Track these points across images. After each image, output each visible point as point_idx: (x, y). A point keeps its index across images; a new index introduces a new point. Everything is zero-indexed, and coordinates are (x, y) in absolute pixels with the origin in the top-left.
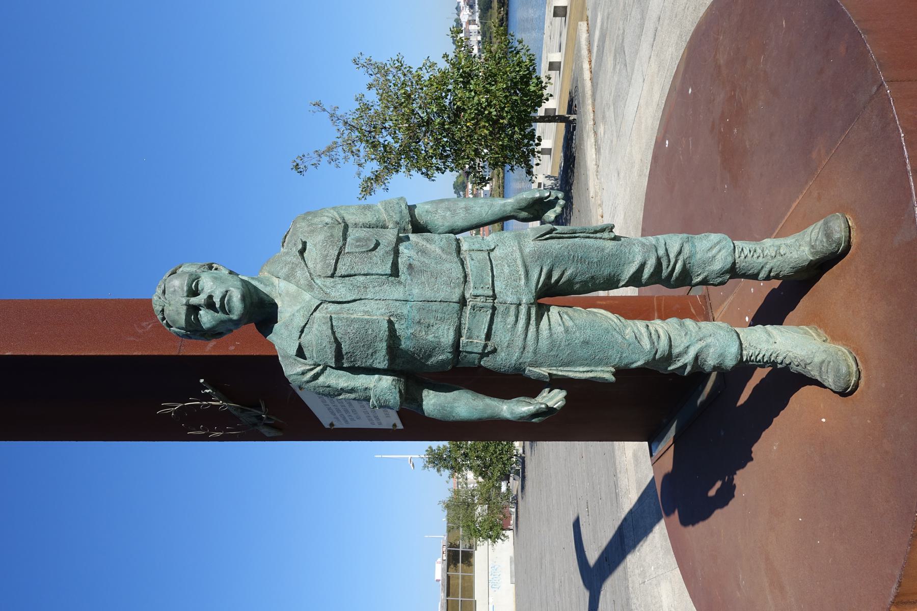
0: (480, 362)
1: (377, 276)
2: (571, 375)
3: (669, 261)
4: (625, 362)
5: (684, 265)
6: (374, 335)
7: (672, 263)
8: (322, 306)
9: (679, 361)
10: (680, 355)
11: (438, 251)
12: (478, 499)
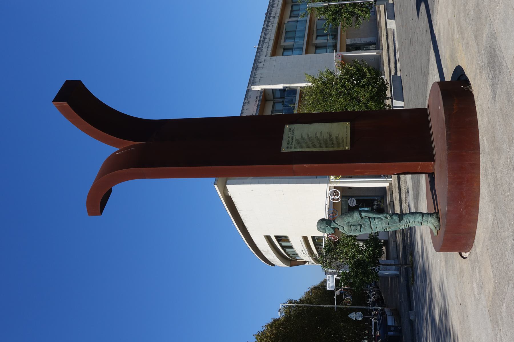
11: (367, 228)
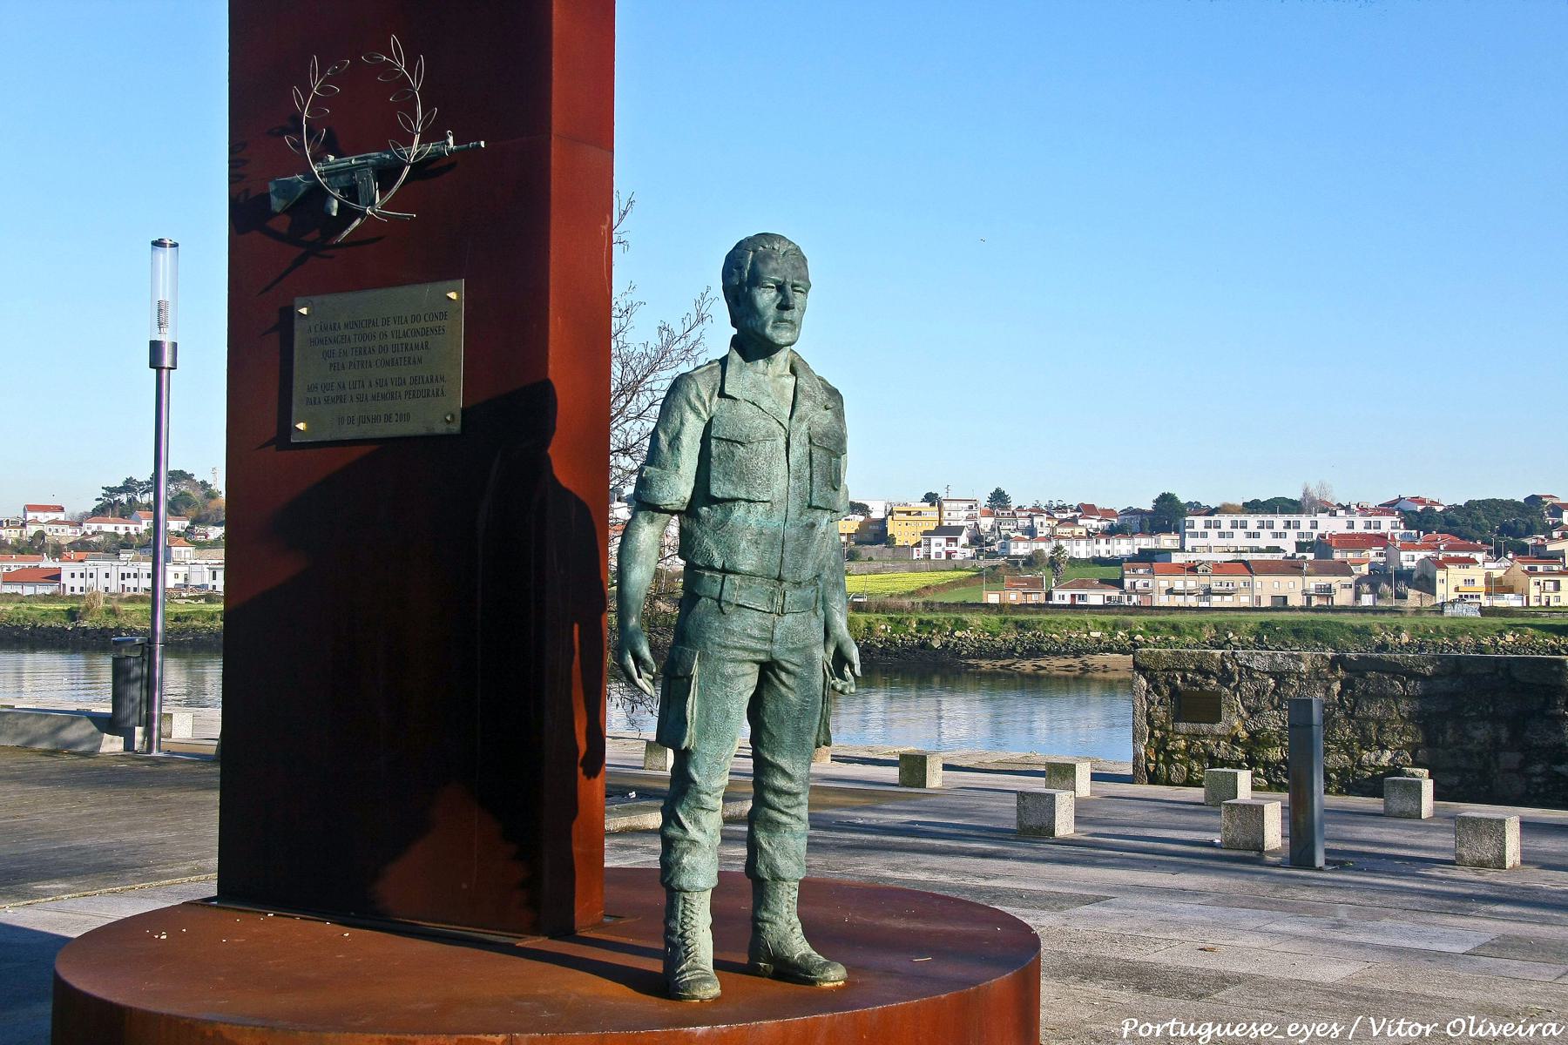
0: (705, 596)
1: (809, 490)
2: (690, 699)
3: (788, 807)
4: (699, 761)
5: (785, 825)
6: (756, 485)
7: (787, 811)
8: (783, 430)
9: (690, 822)
10: (697, 821)
12: (1268, 685)
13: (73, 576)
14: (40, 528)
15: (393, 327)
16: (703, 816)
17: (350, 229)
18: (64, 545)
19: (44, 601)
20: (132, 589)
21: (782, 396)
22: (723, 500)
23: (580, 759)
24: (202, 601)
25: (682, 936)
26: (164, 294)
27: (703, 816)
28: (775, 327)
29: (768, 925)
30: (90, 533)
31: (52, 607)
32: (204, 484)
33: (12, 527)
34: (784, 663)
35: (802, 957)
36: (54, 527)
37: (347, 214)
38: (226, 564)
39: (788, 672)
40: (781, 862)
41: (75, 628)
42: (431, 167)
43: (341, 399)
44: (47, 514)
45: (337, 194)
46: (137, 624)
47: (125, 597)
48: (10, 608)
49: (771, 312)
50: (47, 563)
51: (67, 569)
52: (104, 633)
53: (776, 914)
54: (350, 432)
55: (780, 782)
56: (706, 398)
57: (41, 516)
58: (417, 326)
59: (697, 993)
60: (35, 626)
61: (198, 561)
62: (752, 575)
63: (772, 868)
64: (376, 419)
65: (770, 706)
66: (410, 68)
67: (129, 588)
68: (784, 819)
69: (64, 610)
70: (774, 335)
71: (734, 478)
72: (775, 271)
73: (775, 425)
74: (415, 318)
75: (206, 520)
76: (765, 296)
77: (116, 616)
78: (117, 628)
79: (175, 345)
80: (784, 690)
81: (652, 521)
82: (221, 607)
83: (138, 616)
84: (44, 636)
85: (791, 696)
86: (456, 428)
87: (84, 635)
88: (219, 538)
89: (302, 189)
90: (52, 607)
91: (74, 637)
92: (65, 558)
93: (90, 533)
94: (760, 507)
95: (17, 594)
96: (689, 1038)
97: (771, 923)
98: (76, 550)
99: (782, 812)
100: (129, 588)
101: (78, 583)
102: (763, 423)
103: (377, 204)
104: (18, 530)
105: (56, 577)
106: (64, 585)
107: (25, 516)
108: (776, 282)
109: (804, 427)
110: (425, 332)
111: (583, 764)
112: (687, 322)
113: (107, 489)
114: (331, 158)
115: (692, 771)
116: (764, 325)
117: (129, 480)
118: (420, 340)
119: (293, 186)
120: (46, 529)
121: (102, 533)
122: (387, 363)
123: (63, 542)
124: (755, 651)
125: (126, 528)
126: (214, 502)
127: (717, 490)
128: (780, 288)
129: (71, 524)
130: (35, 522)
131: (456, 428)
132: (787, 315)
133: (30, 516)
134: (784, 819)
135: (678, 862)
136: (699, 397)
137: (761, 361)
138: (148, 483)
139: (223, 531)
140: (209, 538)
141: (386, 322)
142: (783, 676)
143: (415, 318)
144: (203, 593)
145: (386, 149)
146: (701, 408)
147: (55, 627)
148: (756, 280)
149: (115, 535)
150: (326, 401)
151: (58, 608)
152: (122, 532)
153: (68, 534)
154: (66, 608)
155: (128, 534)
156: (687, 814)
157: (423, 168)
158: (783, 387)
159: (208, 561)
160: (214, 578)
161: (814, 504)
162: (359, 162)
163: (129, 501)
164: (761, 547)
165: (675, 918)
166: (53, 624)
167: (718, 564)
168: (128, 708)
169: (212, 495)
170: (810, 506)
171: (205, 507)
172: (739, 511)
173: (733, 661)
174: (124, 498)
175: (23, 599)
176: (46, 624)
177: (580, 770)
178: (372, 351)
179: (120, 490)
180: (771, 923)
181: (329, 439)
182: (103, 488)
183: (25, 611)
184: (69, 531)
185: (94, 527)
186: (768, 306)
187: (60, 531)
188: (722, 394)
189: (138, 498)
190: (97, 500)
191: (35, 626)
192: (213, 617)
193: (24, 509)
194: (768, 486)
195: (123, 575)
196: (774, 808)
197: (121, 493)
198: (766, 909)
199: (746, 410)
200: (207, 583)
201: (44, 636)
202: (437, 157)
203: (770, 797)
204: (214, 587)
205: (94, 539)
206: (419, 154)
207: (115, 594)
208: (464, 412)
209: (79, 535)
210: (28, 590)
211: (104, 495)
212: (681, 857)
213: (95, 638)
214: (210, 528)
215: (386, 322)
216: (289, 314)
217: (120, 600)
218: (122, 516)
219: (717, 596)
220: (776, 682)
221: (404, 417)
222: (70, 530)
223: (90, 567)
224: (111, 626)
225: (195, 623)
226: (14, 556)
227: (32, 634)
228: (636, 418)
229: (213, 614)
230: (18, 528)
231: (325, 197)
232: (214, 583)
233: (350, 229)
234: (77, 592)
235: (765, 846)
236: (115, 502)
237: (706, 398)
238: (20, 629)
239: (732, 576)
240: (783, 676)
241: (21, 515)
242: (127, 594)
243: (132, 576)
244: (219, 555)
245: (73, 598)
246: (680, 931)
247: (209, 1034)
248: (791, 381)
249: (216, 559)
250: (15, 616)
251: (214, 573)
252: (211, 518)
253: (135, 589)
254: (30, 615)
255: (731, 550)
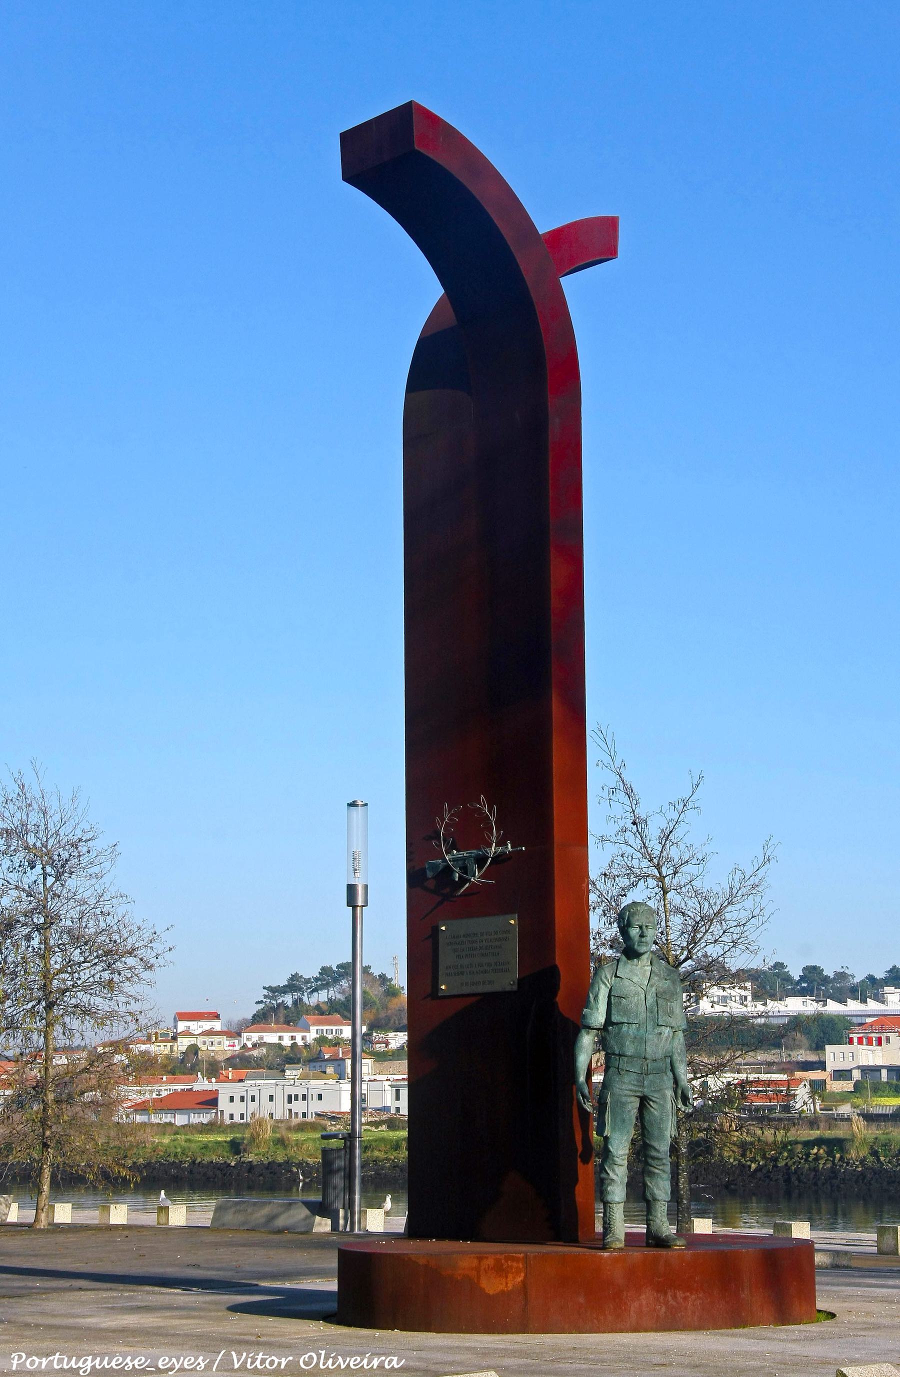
5: (658, 1174)
13: (232, 1099)
14: (193, 1041)
15: (485, 937)
16: (616, 1168)
17: (464, 888)
18: (220, 1062)
19: (201, 1132)
20: (300, 1115)
21: (644, 975)
22: (617, 1024)
23: (578, 1154)
24: (384, 1127)
25: (609, 1224)
26: (357, 847)
27: (616, 1168)
28: (638, 945)
29: (652, 1222)
30: (250, 1046)
31: (211, 1138)
32: (383, 978)
33: (162, 1041)
34: (651, 1097)
35: (666, 1236)
36: (208, 1039)
37: (462, 881)
38: (409, 1079)
39: (653, 1101)
40: (656, 1191)
41: (240, 1164)
42: (500, 858)
43: (462, 973)
44: (201, 1023)
45: (457, 870)
46: (310, 1156)
47: (293, 1124)
48: (166, 1140)
49: (637, 938)
50: (202, 1084)
51: (225, 1091)
52: (272, 1168)
53: (656, 1216)
54: (466, 990)
55: (654, 1153)
56: (609, 978)
57: (196, 1027)
58: (496, 936)
59: (612, 1246)
60: (194, 1162)
61: (378, 1077)
62: (631, 1056)
63: (653, 1195)
64: (478, 983)
65: (647, 1118)
66: (490, 811)
67: (297, 1114)
68: (657, 1171)
69: (226, 1142)
70: (638, 949)
71: (621, 1013)
72: (638, 920)
73: (640, 989)
74: (495, 933)
75: (387, 1025)
76: (634, 932)
77: (285, 1147)
78: (287, 1162)
79: (366, 887)
80: (652, 1110)
81: (588, 1033)
82: (404, 1134)
83: (310, 1146)
84: (205, 1174)
85: (656, 1113)
86: (515, 988)
87: (249, 1171)
88: (402, 1047)
89: (441, 867)
90: (211, 1138)
91: (238, 1175)
92: (222, 1077)
93: (250, 1046)
94: (634, 1026)
95: (170, 1124)
96: (601, 1257)
97: (654, 1221)
98: (235, 1068)
99: (655, 1168)
100: (297, 1114)
101: (237, 1109)
102: (634, 988)
103: (476, 876)
104: (169, 1044)
105: (211, 1101)
106: (222, 1112)
107: (176, 1027)
108: (638, 925)
109: (654, 989)
110: (500, 939)
111: (580, 1157)
112: (755, 863)
113: (270, 989)
114: (455, 852)
115: (610, 1147)
116: (634, 945)
117: (295, 977)
118: (498, 943)
119: (436, 866)
120: (199, 1042)
121: (265, 1044)
122: (483, 955)
123: (220, 1058)
124: (636, 1091)
125: (293, 1038)
126: (395, 1001)
127: (615, 1018)
128: (641, 927)
129: (228, 1034)
130: (187, 1033)
131: (515, 988)
132: (643, 940)
133: (182, 1026)
134: (657, 1171)
135: (606, 1190)
136: (606, 978)
137: (635, 960)
138: (317, 979)
139: (406, 1038)
140: (390, 1046)
141: (482, 934)
142: (651, 1103)
143: (495, 933)
144: (384, 1117)
145: (480, 849)
146: (607, 983)
147: (217, 1163)
148: (629, 925)
149: (280, 1047)
150: (455, 974)
151: (219, 1139)
152: (287, 1042)
153: (224, 1047)
154: (228, 1139)
155: (294, 1045)
156: (609, 1167)
157: (497, 859)
158: (645, 971)
159: (390, 1077)
160: (398, 1098)
161: (660, 1024)
162: (468, 855)
163: (295, 1003)
164: (636, 1044)
165: (606, 1216)
166: (214, 1159)
167: (617, 1052)
168: (332, 1195)
169: (392, 992)
170: (658, 1025)
171: (385, 1007)
172: (625, 1028)
173: (625, 1096)
174: (288, 999)
175: (178, 1130)
176: (207, 1159)
177: (579, 1160)
178: (476, 949)
179: (283, 990)
180: (654, 1221)
181: (456, 994)
182: (264, 988)
183: (183, 1143)
184: (226, 1042)
185: (255, 1037)
186: (635, 936)
187: (215, 1043)
188: (616, 976)
189: (305, 999)
190: (258, 1003)
191: (194, 1162)
192: (396, 1147)
193: (175, 1018)
194: (637, 1016)
195: (290, 1096)
196: (651, 1166)
197: (285, 993)
198: (651, 1215)
199: (627, 982)
200: (389, 1105)
201: (205, 1174)
202: (503, 854)
203: (650, 1161)
204: (398, 1109)
205: (255, 1053)
206: (495, 852)
207: (281, 1121)
208: (519, 980)
209: (237, 1048)
210: (180, 1120)
211: (265, 997)
212: (607, 1187)
213: (261, 1175)
214: (391, 1035)
215: (482, 934)
216: (436, 929)
217: (289, 1129)
218: (287, 1023)
219: (617, 1067)
220: (648, 1106)
221: (491, 982)
222: (227, 1043)
223: (250, 1086)
224: (280, 1159)
225: (377, 1153)
226: (165, 1078)
227: (191, 1172)
228: (713, 943)
229: (397, 1141)
230: (168, 1041)
231: (452, 871)
232: (398, 1104)
233: (464, 888)
234: (237, 1119)
235: (649, 1184)
236: (279, 1005)
237: (609, 978)
238: (177, 1165)
239: (623, 1057)
240: (651, 1103)
241: (171, 1025)
242: (295, 1121)
243: (300, 1097)
244: (400, 1072)
245: (233, 1126)
246: (608, 1221)
247: (406, 1259)
248: (649, 968)
249: (400, 1073)
250: (173, 1149)
251: (398, 1092)
252: (392, 1021)
253: (304, 1115)
254: (189, 1148)
255: (622, 1045)
